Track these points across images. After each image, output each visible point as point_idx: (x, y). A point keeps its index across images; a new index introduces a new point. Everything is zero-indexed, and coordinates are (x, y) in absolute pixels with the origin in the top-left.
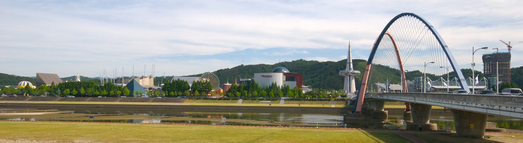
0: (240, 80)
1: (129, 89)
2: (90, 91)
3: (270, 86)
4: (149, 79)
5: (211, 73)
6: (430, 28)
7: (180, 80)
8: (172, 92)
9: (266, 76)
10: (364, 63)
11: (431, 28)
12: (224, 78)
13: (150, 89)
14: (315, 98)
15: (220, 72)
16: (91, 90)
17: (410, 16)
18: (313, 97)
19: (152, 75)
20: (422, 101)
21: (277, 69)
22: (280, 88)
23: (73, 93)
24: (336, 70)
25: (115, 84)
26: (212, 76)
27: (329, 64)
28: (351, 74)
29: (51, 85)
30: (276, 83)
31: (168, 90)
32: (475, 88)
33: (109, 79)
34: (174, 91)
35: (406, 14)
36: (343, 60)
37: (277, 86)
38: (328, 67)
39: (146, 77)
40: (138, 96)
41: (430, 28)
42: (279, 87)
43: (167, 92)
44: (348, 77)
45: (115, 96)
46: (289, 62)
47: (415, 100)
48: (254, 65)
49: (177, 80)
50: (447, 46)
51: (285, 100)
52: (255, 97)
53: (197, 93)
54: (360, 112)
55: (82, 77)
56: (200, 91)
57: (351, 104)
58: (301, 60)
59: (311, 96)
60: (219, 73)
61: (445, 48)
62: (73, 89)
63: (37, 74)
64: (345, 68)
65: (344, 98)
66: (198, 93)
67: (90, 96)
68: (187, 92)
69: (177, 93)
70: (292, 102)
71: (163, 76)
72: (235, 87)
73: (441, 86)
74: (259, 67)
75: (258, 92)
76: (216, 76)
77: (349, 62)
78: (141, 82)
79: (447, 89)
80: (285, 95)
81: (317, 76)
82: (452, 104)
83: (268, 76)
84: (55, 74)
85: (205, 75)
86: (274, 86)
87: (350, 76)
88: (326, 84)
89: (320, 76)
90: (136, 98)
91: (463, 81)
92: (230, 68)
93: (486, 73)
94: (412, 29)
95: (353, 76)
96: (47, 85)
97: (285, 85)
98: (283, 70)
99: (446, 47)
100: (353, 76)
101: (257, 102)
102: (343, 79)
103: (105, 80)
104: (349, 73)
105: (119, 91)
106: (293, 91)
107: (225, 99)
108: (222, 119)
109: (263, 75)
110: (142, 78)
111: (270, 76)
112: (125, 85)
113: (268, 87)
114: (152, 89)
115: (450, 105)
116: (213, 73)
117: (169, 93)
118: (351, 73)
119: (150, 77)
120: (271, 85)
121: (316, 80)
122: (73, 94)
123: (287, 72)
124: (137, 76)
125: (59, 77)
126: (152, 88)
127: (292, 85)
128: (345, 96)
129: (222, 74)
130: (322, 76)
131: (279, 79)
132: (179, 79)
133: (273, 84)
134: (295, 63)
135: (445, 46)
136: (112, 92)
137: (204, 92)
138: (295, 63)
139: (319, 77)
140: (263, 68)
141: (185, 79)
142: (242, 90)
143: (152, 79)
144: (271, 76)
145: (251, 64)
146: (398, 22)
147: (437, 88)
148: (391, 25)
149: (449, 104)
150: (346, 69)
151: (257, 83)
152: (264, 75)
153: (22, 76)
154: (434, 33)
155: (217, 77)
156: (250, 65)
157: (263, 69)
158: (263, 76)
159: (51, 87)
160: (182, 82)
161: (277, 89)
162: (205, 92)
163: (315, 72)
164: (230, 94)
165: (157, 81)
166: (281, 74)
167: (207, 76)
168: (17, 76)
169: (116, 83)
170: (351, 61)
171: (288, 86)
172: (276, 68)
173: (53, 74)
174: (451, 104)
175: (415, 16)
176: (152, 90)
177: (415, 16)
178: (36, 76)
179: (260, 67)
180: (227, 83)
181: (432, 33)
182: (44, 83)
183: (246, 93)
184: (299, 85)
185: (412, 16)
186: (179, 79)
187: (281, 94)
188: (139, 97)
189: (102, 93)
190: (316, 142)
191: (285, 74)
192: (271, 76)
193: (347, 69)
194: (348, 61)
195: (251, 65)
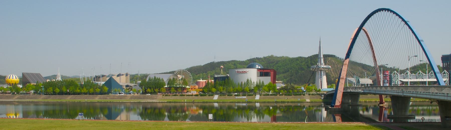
0: (215, 77)
1: (108, 87)
4: (126, 76)
5: (184, 70)
6: (406, 23)
7: (156, 77)
9: (240, 72)
10: (334, 58)
16: (72, 88)
17: (387, 11)
20: (412, 94)
21: (252, 64)
23: (56, 91)
25: (94, 82)
26: (185, 72)
28: (323, 69)
29: (36, 84)
32: (410, 81)
33: (88, 78)
38: (298, 62)
39: (123, 75)
41: (406, 23)
44: (320, 72)
45: (94, 93)
50: (422, 41)
54: (340, 106)
55: (62, 77)
59: (285, 91)
61: (421, 42)
64: (316, 63)
65: (318, 93)
67: (72, 94)
69: (154, 90)
75: (233, 88)
76: (189, 73)
77: (320, 57)
78: (117, 79)
79: (408, 82)
83: (243, 72)
84: (39, 74)
85: (178, 72)
87: (321, 71)
88: (297, 79)
90: (388, 96)
91: (438, 73)
93: (445, 66)
95: (324, 70)
96: (32, 84)
97: (260, 81)
99: (422, 41)
100: (324, 70)
102: (313, 74)
103: (84, 78)
111: (245, 72)
112: (104, 83)
113: (243, 83)
114: (128, 87)
115: (446, 97)
116: (185, 70)
119: (127, 75)
122: (56, 92)
123: (261, 68)
124: (105, 74)
125: (42, 77)
127: (267, 80)
128: (319, 91)
132: (155, 78)
133: (248, 80)
135: (421, 40)
141: (161, 77)
144: (245, 72)
146: (373, 19)
147: (404, 81)
148: (368, 20)
149: (444, 96)
154: (410, 27)
155: (190, 73)
157: (236, 65)
162: (181, 89)
165: (133, 78)
167: (180, 73)
169: (94, 81)
170: (322, 56)
171: (263, 82)
172: (250, 64)
173: (37, 74)
174: (447, 96)
175: (391, 11)
177: (391, 11)
181: (408, 27)
182: (29, 83)
184: (274, 80)
185: (388, 11)
186: (155, 78)
191: (258, 69)
195: (223, 61)
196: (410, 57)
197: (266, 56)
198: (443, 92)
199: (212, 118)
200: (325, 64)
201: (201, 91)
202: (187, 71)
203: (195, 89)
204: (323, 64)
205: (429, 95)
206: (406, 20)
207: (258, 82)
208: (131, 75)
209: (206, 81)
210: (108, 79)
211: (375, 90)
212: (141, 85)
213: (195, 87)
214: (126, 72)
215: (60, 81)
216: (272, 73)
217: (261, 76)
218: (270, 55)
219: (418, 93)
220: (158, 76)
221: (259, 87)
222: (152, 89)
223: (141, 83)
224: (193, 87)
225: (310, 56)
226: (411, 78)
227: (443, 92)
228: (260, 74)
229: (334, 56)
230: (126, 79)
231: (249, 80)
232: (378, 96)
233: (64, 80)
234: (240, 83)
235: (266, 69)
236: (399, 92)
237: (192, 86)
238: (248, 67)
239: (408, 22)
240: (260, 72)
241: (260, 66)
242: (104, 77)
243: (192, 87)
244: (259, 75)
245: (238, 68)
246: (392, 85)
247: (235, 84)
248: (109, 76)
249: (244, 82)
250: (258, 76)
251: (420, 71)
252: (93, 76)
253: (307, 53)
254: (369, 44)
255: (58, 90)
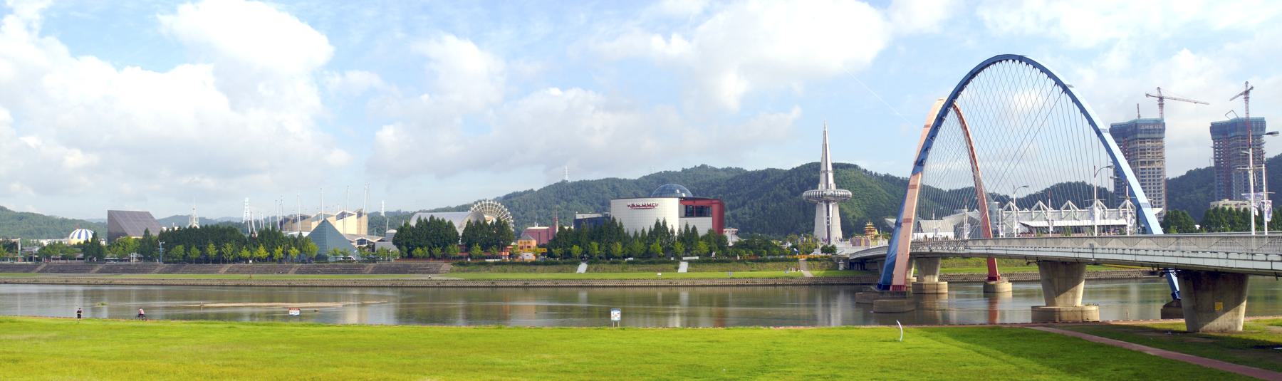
0: (577, 218)
2: (229, 249)
3: (650, 229)
4: (357, 218)
6: (1065, 89)
7: (436, 218)
8: (418, 248)
9: (639, 206)
11: (1070, 88)
12: (522, 214)
13: (361, 242)
14: (762, 256)
15: (513, 199)
18: (756, 254)
19: (362, 209)
22: (676, 234)
24: (788, 189)
27: (771, 174)
29: (141, 238)
30: (664, 223)
31: (407, 245)
32: (1099, 224)
34: (421, 247)
35: (1006, 58)
36: (802, 166)
37: (667, 229)
39: (350, 215)
40: (338, 259)
41: (1065, 89)
42: (673, 232)
43: (405, 248)
44: (824, 205)
46: (675, 173)
47: (1093, 253)
48: (592, 181)
49: (428, 220)
51: (690, 262)
52: (615, 257)
53: (477, 250)
55: (201, 219)
56: (485, 247)
57: (845, 269)
58: (703, 166)
60: (511, 202)
62: (190, 248)
63: (110, 214)
64: (815, 183)
66: (479, 251)
67: (230, 262)
68: (455, 250)
70: (707, 266)
71: (185, 214)
72: (569, 234)
73: (1041, 222)
74: (605, 186)
78: (339, 226)
80: (688, 252)
81: (744, 204)
82: (1268, 259)
83: (645, 206)
86: (660, 229)
88: (766, 222)
89: (752, 204)
91: (1146, 207)
92: (536, 189)
94: (1026, 87)
97: (687, 226)
98: (678, 191)
101: (623, 269)
104: (825, 194)
105: (294, 248)
106: (706, 238)
107: (546, 264)
108: (1164, 280)
109: (633, 205)
110: (342, 216)
113: (647, 231)
116: (494, 200)
117: (429, 251)
118: (831, 195)
119: (360, 215)
120: (653, 227)
121: (743, 214)
126: (365, 240)
127: (704, 225)
129: (517, 203)
130: (755, 204)
131: (669, 212)
132: (432, 218)
133: (657, 224)
134: (691, 174)
136: (278, 252)
137: (494, 248)
138: (691, 174)
139: (750, 205)
140: (614, 188)
141: (447, 217)
142: (584, 240)
143: (365, 219)
144: (651, 206)
145: (586, 179)
150: (820, 185)
151: (620, 223)
152: (635, 203)
153: (70, 218)
156: (582, 180)
157: (619, 188)
158: (633, 206)
159: (142, 241)
160: (441, 223)
161: (669, 237)
163: (739, 196)
164: (557, 251)
165: (376, 224)
166: (676, 201)
168: (61, 217)
170: (830, 168)
171: (694, 228)
172: (658, 185)
176: (365, 246)
178: (106, 217)
179: (607, 185)
180: (534, 226)
183: (596, 248)
186: (432, 218)
187: (679, 247)
188: (340, 261)
189: (256, 254)
190: (670, 378)
191: (683, 200)
192: (651, 206)
193: (822, 186)
194: (823, 168)
196: (1097, 169)
197: (688, 167)
198: (1109, 246)
199: (1221, 303)
200: (839, 186)
201: (543, 254)
202: (498, 203)
203: (529, 247)
204: (833, 186)
205: (1173, 256)
206: (1066, 82)
207: (683, 230)
208: (368, 215)
209: (548, 229)
210: (314, 225)
211: (1005, 248)
212: (397, 241)
213: (529, 242)
214: (358, 208)
215: (196, 227)
216: (715, 208)
217: (686, 215)
218: (698, 165)
219: (1140, 253)
220: (437, 216)
221: (689, 237)
222: (426, 249)
223: (396, 235)
224: (525, 243)
225: (797, 168)
226: (1077, 217)
227: (1109, 246)
228: (686, 212)
229: (855, 166)
230: (357, 229)
231: (661, 222)
232: (984, 261)
233: (204, 225)
234: (639, 232)
235: (699, 199)
236: (1079, 250)
237: (523, 241)
238: (661, 196)
239: (1071, 86)
240: (686, 207)
241: (686, 193)
242: (306, 221)
243: (521, 243)
244: (683, 214)
245: (621, 197)
246: (1128, 235)
247: (628, 233)
248: (317, 218)
249: (649, 227)
250: (680, 217)
251: (1070, 202)
252: (279, 218)
253: (787, 160)
254: (963, 138)
255: (195, 252)
